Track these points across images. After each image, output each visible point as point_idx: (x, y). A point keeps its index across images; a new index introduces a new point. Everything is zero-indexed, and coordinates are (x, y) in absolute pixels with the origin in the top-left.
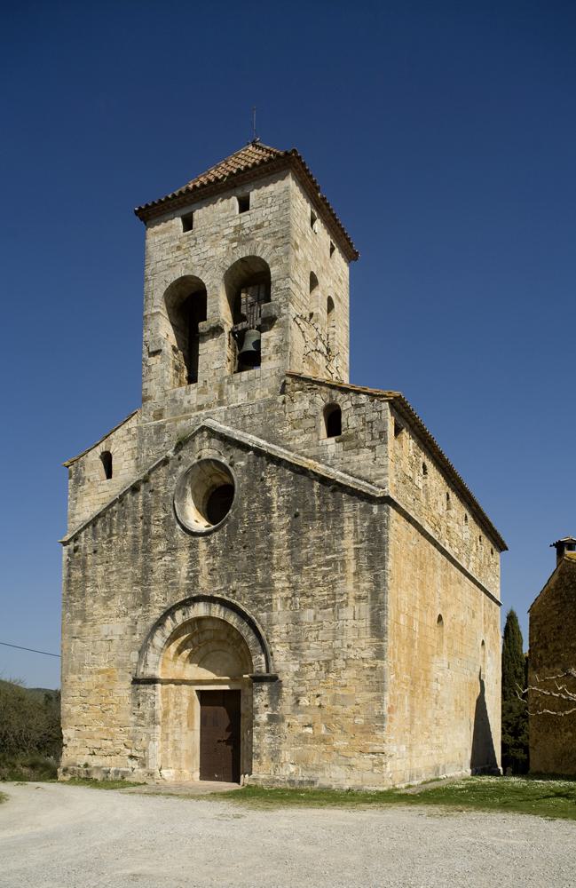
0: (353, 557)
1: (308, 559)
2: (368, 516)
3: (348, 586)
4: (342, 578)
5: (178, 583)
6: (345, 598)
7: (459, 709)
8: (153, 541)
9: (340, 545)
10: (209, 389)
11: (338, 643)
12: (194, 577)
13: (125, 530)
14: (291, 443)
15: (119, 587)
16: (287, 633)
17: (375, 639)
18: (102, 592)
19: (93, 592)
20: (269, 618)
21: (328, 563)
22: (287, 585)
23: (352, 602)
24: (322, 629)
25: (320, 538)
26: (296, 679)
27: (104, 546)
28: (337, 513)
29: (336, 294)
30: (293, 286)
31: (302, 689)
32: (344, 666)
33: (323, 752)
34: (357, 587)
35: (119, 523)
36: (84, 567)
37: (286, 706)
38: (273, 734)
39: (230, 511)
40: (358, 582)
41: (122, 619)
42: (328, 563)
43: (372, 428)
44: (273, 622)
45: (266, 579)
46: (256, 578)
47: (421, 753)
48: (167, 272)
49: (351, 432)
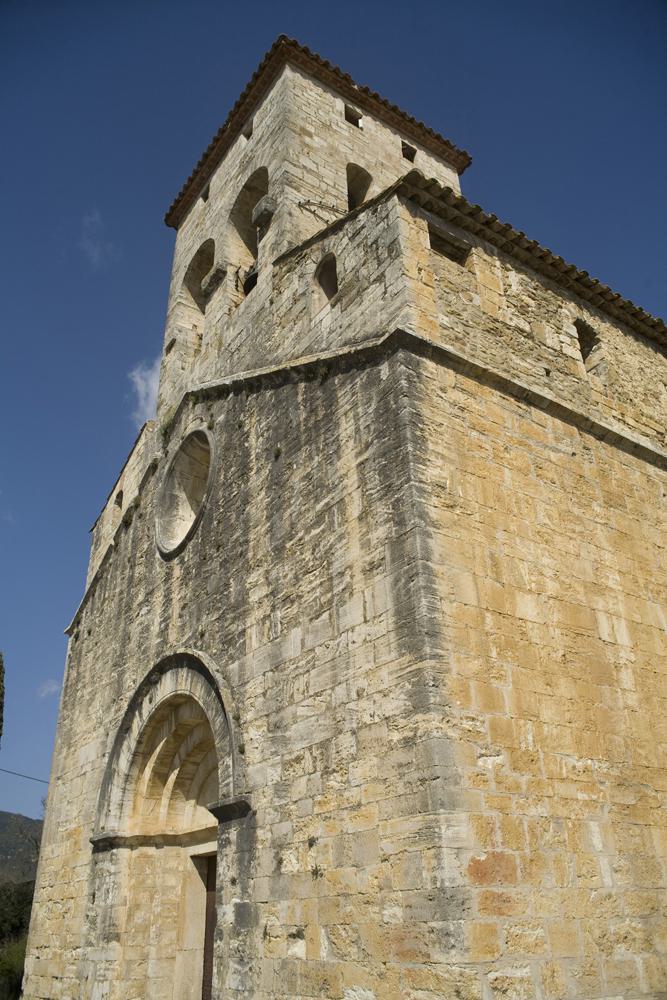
3: (352, 553)
16: (264, 694)
17: (408, 658)
24: (314, 667)
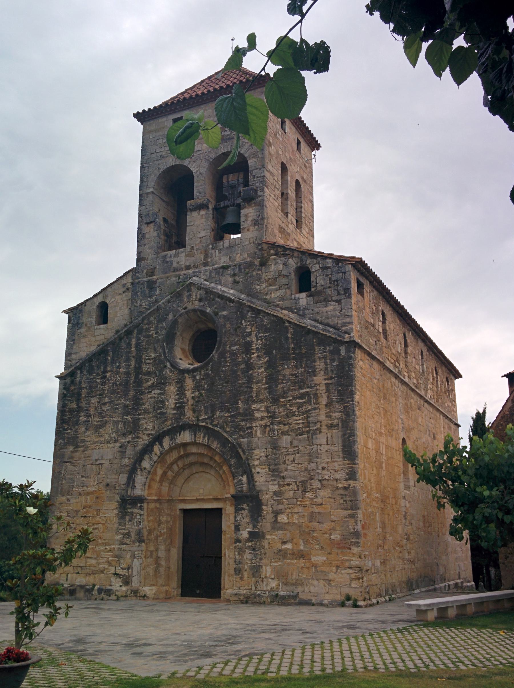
0: (325, 391)
1: (284, 392)
2: (336, 357)
4: (315, 409)
5: (166, 413)
6: (318, 426)
7: (427, 525)
8: (144, 377)
9: (313, 380)
10: (196, 253)
11: (313, 466)
12: (180, 407)
13: (119, 367)
14: (268, 297)
15: (111, 416)
16: (266, 457)
17: (347, 462)
18: (95, 420)
19: (86, 421)
20: (250, 443)
21: (302, 396)
22: (265, 414)
23: (324, 429)
24: (298, 453)
25: (295, 374)
26: (275, 498)
27: (98, 381)
28: (309, 356)
29: (302, 178)
30: (267, 174)
31: (280, 507)
32: (319, 486)
33: (302, 567)
34: (328, 416)
35: (113, 362)
36: (79, 399)
37: (266, 524)
38: (254, 550)
39: (214, 352)
40: (330, 412)
41: (112, 445)
42: (302, 396)
43: (337, 285)
44: (253, 447)
45: (247, 410)
46: (237, 409)
47: (394, 568)
48: (160, 162)
49: (319, 288)
